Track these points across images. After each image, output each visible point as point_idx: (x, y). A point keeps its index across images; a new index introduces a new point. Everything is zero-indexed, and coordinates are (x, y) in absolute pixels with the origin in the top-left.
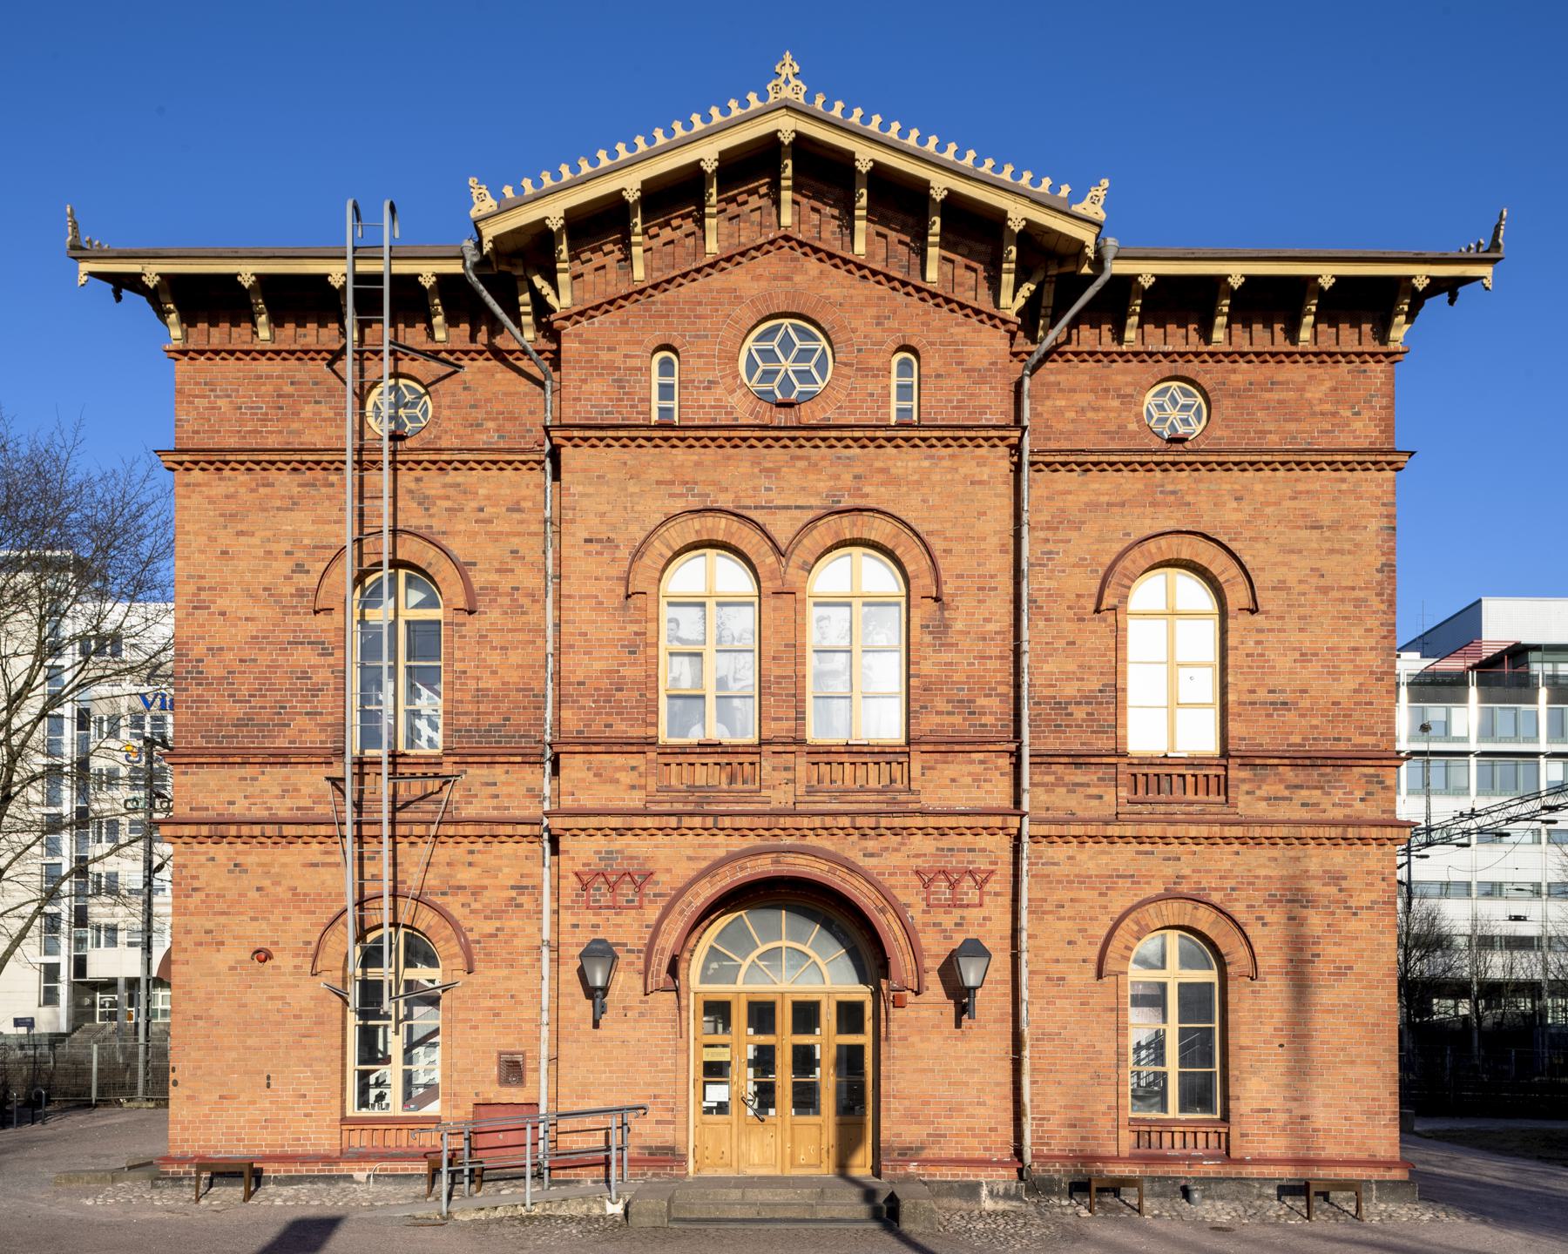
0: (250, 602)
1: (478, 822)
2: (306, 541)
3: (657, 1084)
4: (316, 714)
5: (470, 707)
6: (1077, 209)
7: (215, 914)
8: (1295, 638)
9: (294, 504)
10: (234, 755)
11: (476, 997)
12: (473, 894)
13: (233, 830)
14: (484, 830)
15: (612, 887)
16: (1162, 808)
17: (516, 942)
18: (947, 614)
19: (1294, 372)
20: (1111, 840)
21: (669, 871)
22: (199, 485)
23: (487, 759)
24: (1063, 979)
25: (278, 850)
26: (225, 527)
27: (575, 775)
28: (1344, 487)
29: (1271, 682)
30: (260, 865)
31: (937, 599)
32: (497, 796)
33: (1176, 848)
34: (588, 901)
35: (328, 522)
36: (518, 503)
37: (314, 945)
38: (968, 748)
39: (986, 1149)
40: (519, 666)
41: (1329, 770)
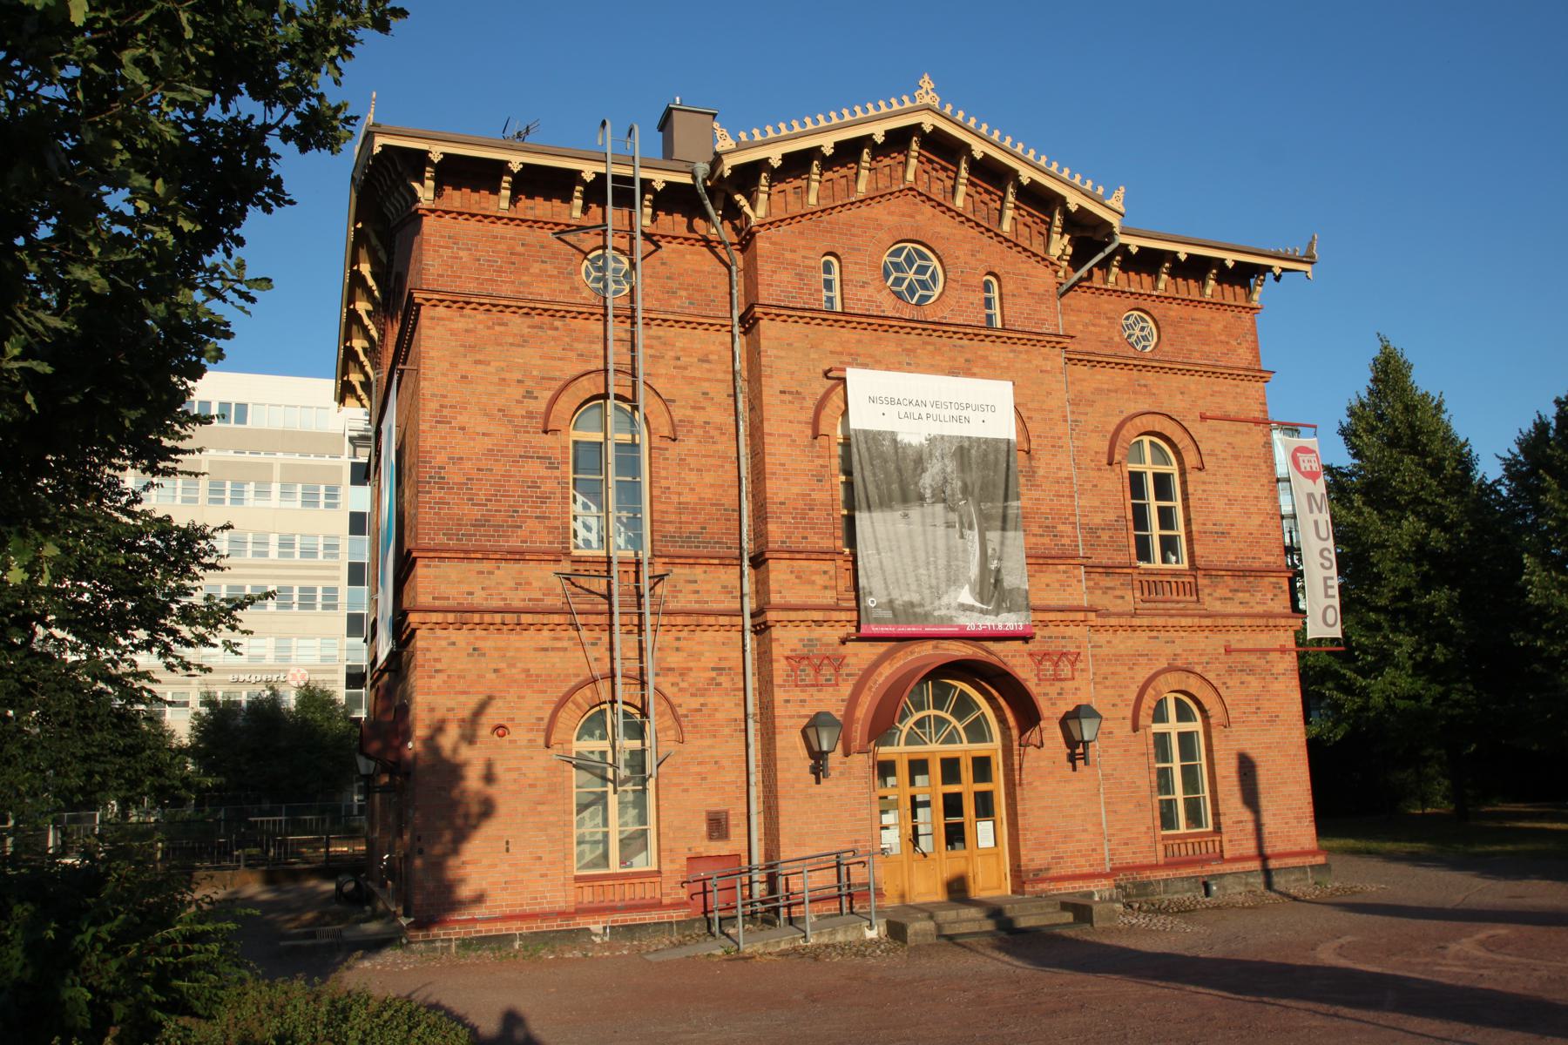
0: (485, 419)
1: (688, 613)
2: (535, 373)
3: (858, 831)
4: (544, 518)
5: (673, 517)
6: (1108, 202)
7: (456, 693)
8: (1223, 488)
9: (524, 342)
10: (475, 552)
11: (687, 764)
12: (681, 674)
13: (476, 618)
14: (692, 620)
15: (817, 669)
16: (1161, 605)
17: (719, 715)
18: (1033, 463)
19: (1204, 314)
20: (1133, 628)
21: (856, 655)
22: (443, 319)
23: (692, 561)
24: (1111, 733)
25: (513, 637)
26: (465, 356)
27: (782, 577)
28: (1239, 390)
29: (1214, 518)
30: (497, 649)
31: (1028, 452)
32: (697, 592)
33: (1172, 634)
34: (796, 680)
35: (553, 358)
36: (707, 355)
37: (546, 721)
38: (1056, 561)
39: (1091, 865)
40: (712, 486)
41: (1252, 579)
